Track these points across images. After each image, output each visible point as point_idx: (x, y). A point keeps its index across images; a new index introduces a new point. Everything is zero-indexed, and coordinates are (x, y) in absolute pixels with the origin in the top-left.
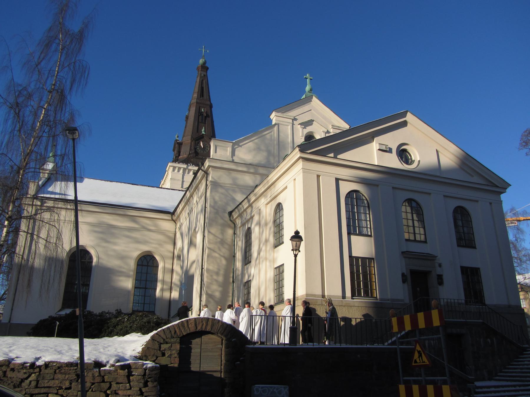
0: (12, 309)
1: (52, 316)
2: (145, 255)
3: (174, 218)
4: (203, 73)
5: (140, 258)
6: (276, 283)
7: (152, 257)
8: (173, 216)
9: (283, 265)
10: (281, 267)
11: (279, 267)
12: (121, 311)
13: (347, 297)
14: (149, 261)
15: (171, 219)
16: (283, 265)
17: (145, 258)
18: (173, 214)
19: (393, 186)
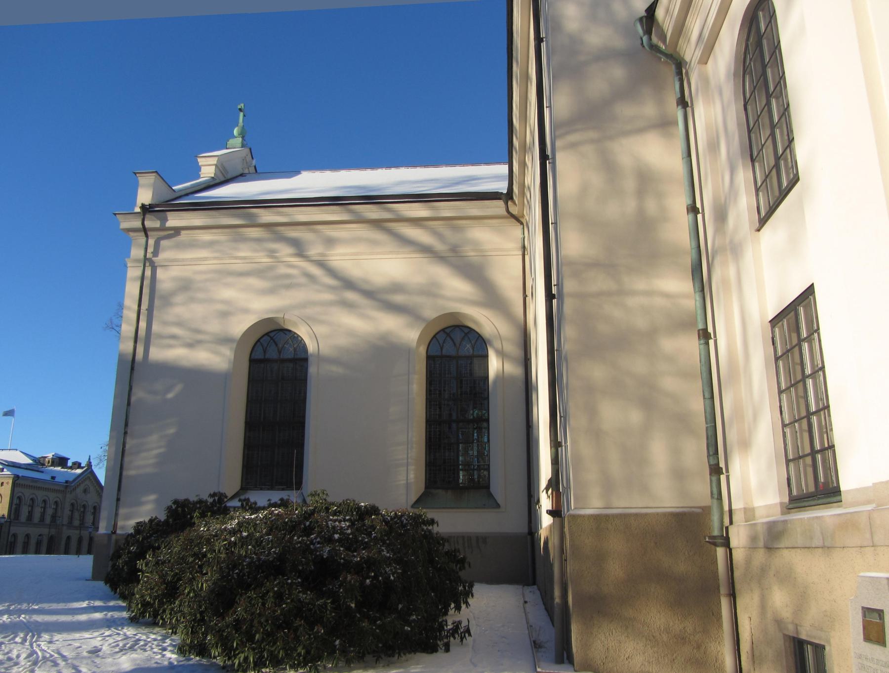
0: (126, 425)
1: (399, 655)
2: (446, 328)
3: (514, 210)
4: (119, 497)
5: (434, 336)
6: (784, 396)
7: (466, 331)
8: (510, 203)
9: (810, 291)
10: (801, 310)
11: (792, 308)
12: (346, 663)
13: (848, 491)
14: (459, 347)
15: (505, 213)
16: (810, 291)
17: (448, 335)
18: (508, 196)
19: (87, 650)
